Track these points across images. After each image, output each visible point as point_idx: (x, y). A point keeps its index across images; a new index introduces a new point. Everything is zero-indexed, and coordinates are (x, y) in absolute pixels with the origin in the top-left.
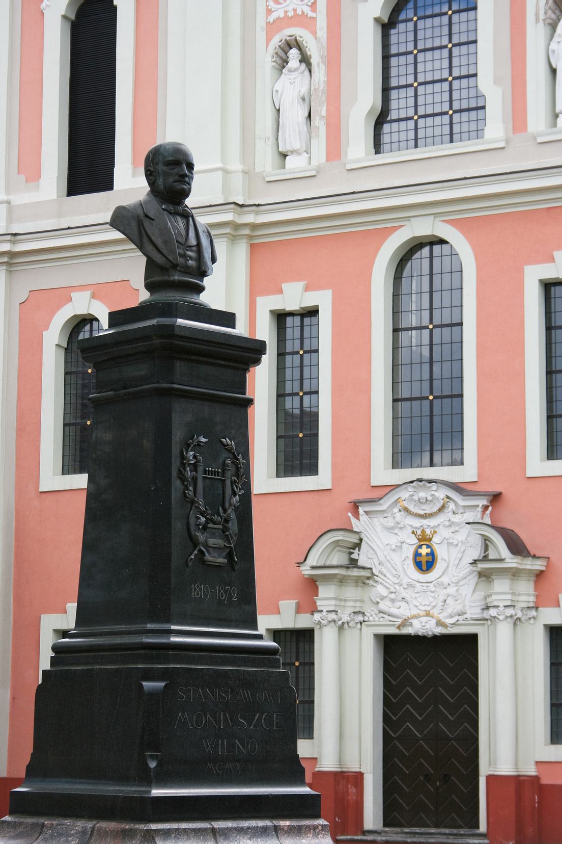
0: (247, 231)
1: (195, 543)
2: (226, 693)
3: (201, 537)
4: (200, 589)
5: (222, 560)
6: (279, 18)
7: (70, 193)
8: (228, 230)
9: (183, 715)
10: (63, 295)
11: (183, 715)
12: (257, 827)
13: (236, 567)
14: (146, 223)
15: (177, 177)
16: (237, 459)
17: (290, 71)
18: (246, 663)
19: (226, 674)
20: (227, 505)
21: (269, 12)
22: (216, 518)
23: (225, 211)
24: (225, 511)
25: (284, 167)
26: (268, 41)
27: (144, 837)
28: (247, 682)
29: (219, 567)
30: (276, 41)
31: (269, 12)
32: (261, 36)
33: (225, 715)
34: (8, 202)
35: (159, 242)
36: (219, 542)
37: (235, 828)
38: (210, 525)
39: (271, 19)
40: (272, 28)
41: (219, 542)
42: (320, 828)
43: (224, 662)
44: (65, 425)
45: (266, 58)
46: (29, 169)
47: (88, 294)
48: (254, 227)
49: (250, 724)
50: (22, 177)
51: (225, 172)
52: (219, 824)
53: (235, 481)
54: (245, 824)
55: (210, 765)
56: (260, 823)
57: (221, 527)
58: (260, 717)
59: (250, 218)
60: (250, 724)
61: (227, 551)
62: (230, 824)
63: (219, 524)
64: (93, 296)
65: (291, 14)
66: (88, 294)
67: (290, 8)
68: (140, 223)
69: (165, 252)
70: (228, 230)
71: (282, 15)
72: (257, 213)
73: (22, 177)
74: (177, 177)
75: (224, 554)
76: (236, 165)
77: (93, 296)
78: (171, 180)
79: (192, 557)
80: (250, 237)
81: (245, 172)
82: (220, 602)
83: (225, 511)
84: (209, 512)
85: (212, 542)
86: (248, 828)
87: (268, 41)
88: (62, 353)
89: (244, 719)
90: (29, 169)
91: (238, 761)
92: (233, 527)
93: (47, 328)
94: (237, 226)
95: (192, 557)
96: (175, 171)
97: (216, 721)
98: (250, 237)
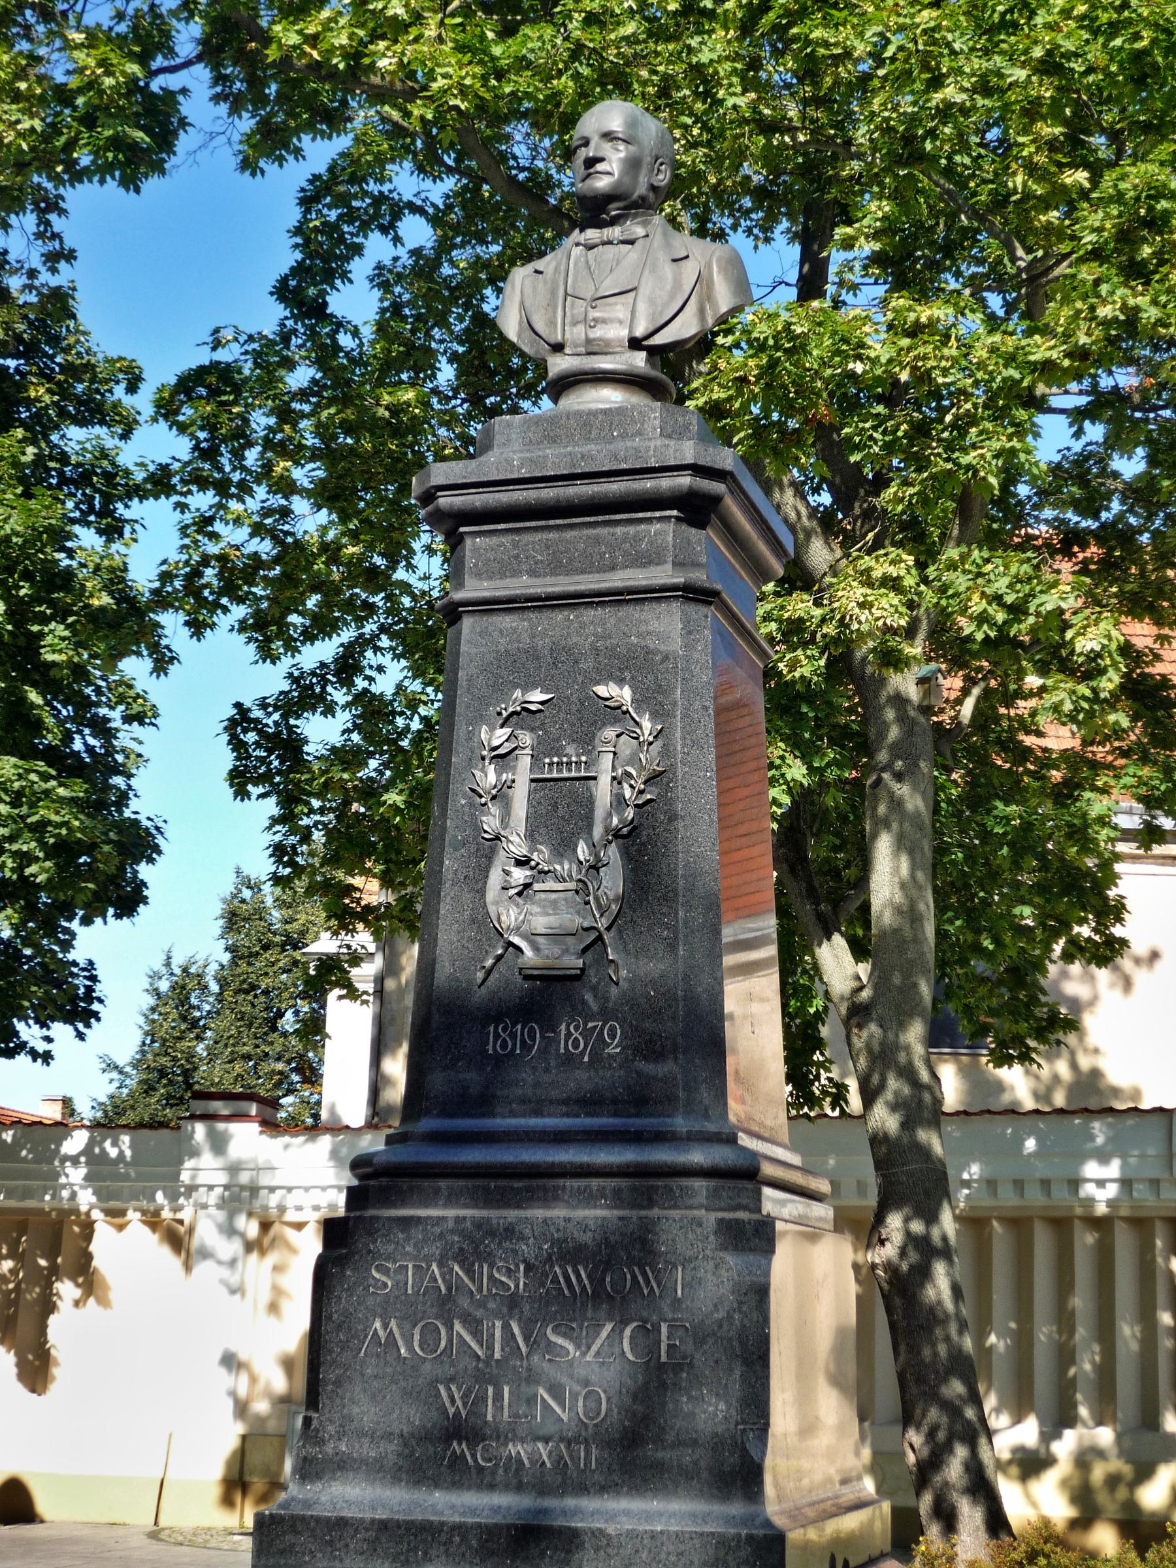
4: (513, 1036)
9: (385, 1326)
33: (506, 1327)
89: (565, 1336)
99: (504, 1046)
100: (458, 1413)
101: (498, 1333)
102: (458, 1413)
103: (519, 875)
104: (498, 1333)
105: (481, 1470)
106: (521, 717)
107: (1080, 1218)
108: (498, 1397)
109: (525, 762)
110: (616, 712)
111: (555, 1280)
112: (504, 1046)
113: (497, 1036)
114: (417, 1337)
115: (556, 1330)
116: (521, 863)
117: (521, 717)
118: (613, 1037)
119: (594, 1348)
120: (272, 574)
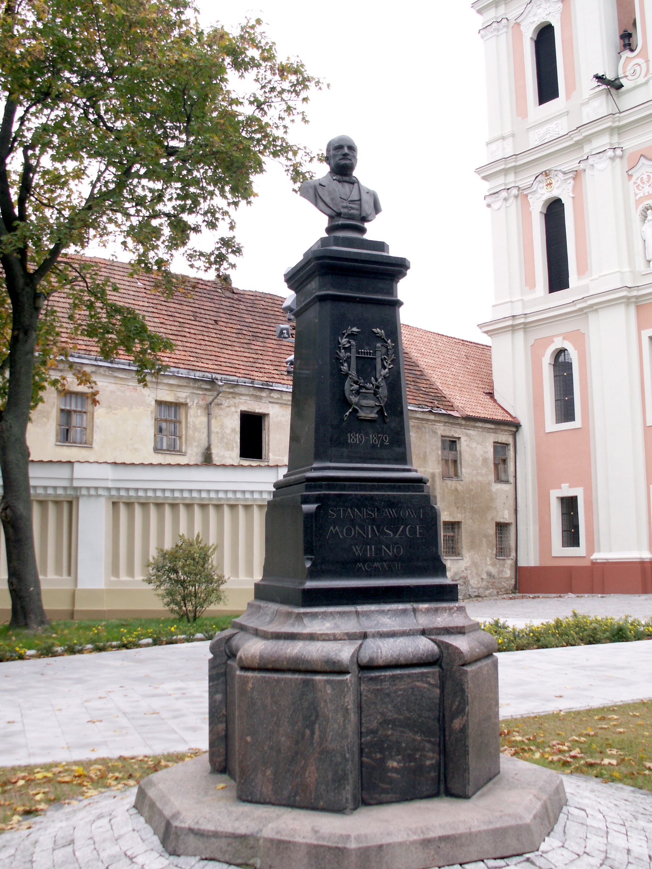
0: (634, 300)
1: (347, 404)
2: (373, 511)
3: (354, 399)
4: (356, 437)
5: (374, 415)
6: (641, 197)
7: (550, 292)
8: (624, 300)
9: (334, 528)
10: (550, 340)
11: (334, 528)
12: (397, 610)
13: (387, 420)
14: (320, 189)
15: (341, 157)
16: (387, 343)
17: (649, 221)
18: (392, 489)
19: (372, 498)
20: (378, 376)
21: (636, 195)
22: (369, 385)
23: (622, 291)
24: (376, 380)
25: (649, 267)
26: (637, 208)
27: (296, 618)
28: (391, 503)
29: (372, 421)
30: (641, 207)
31: (636, 195)
32: (633, 206)
33: (372, 528)
34: (522, 300)
35: (327, 200)
36: (372, 403)
37: (377, 611)
38: (364, 390)
39: (637, 198)
40: (638, 202)
41: (372, 403)
42: (455, 609)
43: (372, 489)
44: (556, 400)
45: (636, 217)
46: (530, 283)
47: (561, 338)
48: (637, 297)
49: (395, 533)
50: (528, 288)
51: (622, 273)
52: (360, 608)
53: (385, 359)
54: (387, 607)
55: (360, 565)
56: (401, 606)
57: (372, 391)
58: (405, 529)
59: (635, 293)
60: (395, 533)
61: (378, 409)
62: (373, 607)
63: (371, 389)
64: (564, 339)
65: (646, 194)
66: (561, 338)
67: (646, 191)
68: (315, 190)
69: (331, 206)
70: (624, 300)
71: (642, 195)
72: (638, 290)
73: (528, 288)
74: (341, 157)
75: (375, 411)
76: (626, 269)
77: (564, 339)
78: (337, 159)
79: (347, 414)
80: (636, 302)
81: (631, 272)
82: (374, 446)
83: (376, 380)
84: (362, 381)
85: (364, 402)
86: (389, 610)
87: (637, 208)
88: (552, 367)
89: (390, 530)
90: (530, 283)
91: (385, 561)
92: (383, 392)
93: (543, 356)
94: (629, 298)
95: (347, 414)
96: (340, 153)
97: (364, 533)
98: (636, 302)
99: (353, 440)
100: (359, 555)
101: (370, 529)
102: (359, 555)
103: (356, 387)
104: (370, 529)
105: (367, 571)
106: (351, 336)
107: (52, 501)
108: (371, 549)
109: (353, 350)
110: (379, 338)
111: (386, 513)
112: (353, 440)
113: (351, 437)
114: (345, 531)
115: (387, 529)
116: (356, 383)
117: (351, 336)
118: (386, 439)
119: (398, 533)
120: (46, 284)
